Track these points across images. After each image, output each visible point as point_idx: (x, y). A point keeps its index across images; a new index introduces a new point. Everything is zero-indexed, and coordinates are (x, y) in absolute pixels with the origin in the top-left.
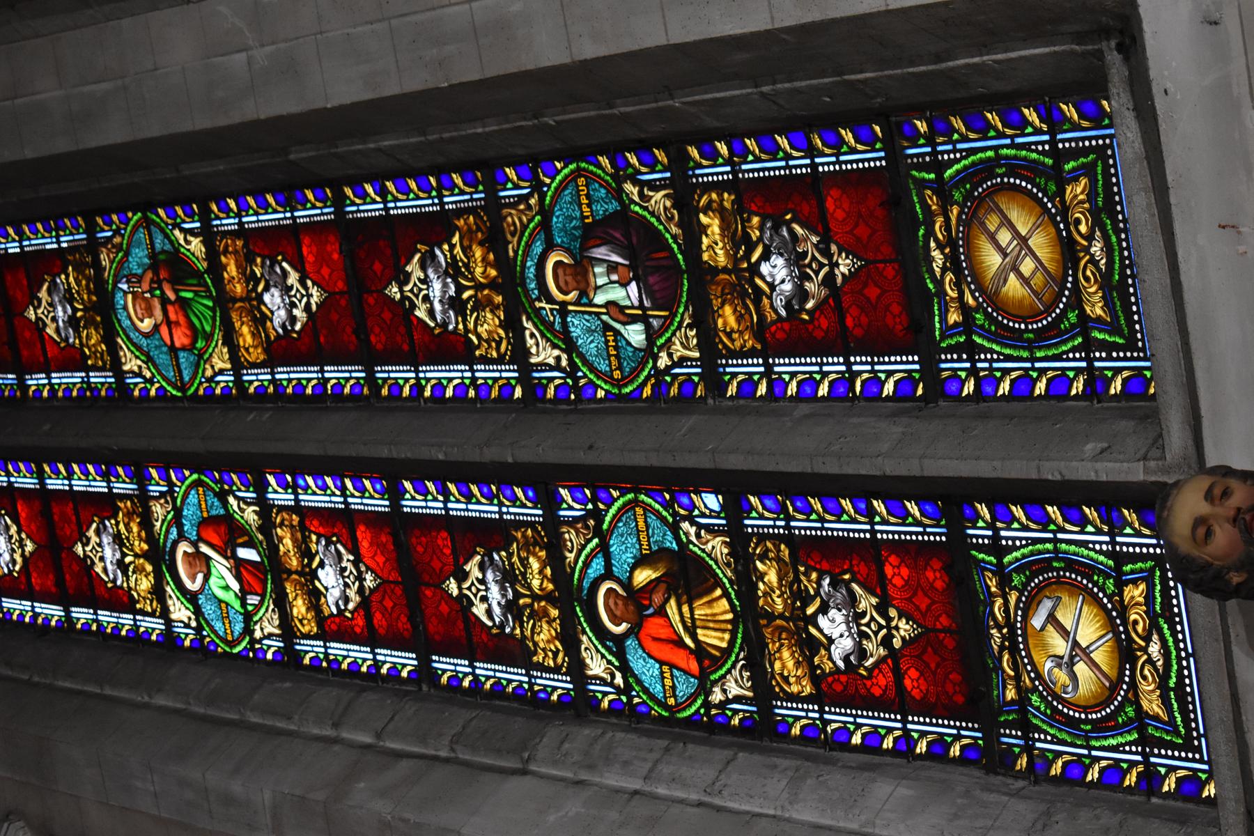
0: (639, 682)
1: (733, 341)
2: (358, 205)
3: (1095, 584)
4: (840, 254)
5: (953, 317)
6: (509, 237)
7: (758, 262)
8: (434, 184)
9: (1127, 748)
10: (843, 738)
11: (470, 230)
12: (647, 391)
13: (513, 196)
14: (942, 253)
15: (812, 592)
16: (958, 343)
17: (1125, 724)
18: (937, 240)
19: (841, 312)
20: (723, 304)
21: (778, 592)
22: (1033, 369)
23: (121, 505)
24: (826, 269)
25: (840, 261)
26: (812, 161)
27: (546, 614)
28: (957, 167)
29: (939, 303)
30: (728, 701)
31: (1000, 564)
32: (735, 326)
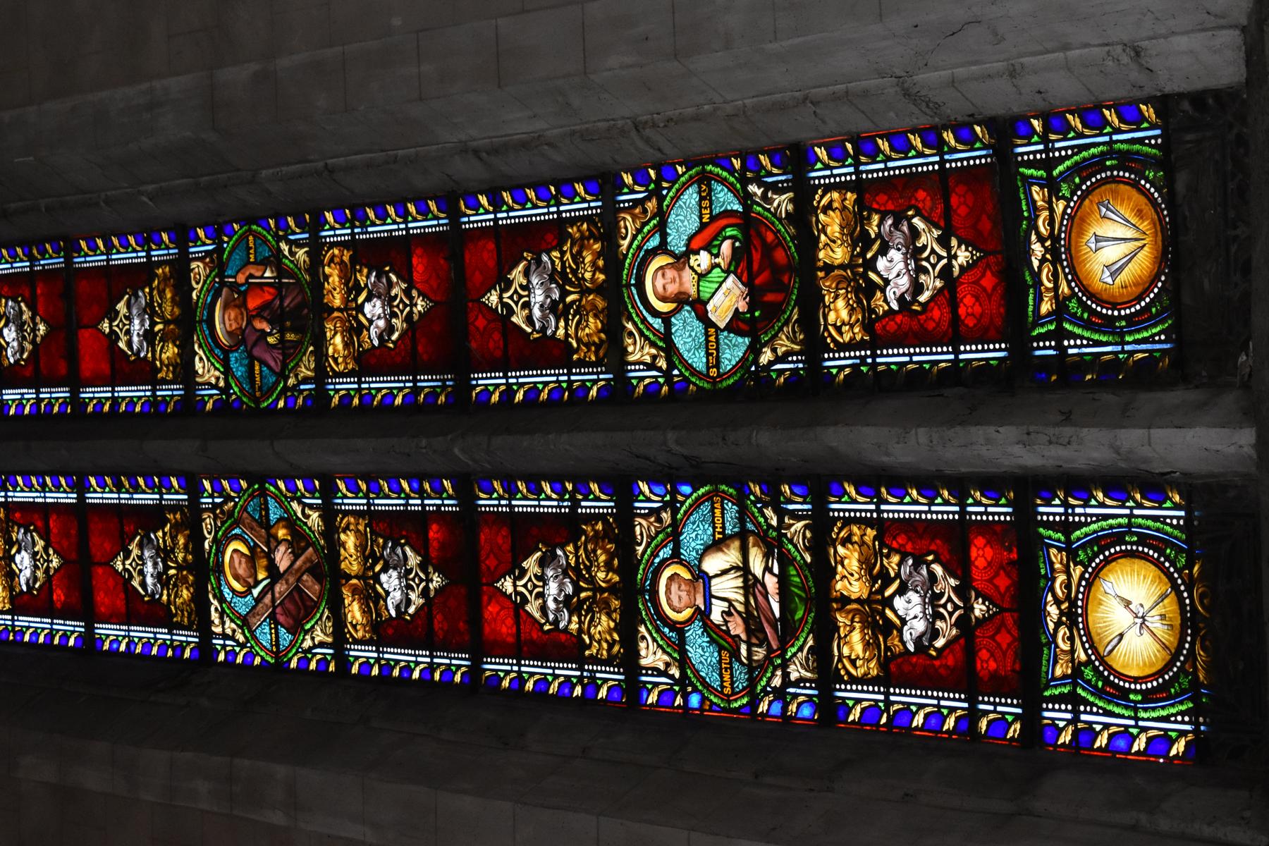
0: (696, 672)
1: (841, 334)
2: (469, 216)
3: (1167, 558)
4: (959, 246)
5: (1045, 307)
6: (194, 283)
7: (875, 258)
8: (1038, 129)
9: (1179, 718)
10: (905, 719)
11: (583, 238)
12: (281, 404)
13: (628, 201)
14: (1043, 246)
15: (892, 574)
16: (1049, 331)
17: (1177, 695)
18: (1038, 234)
19: (954, 304)
20: (836, 297)
21: (856, 576)
22: (1123, 352)
23: (170, 516)
24: (945, 261)
25: (959, 253)
26: (942, 158)
27: (607, 603)
28: (1068, 163)
29: (1035, 294)
30: (315, 646)
31: (1069, 542)
32: (846, 318)
